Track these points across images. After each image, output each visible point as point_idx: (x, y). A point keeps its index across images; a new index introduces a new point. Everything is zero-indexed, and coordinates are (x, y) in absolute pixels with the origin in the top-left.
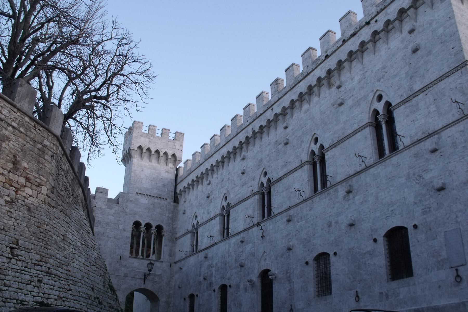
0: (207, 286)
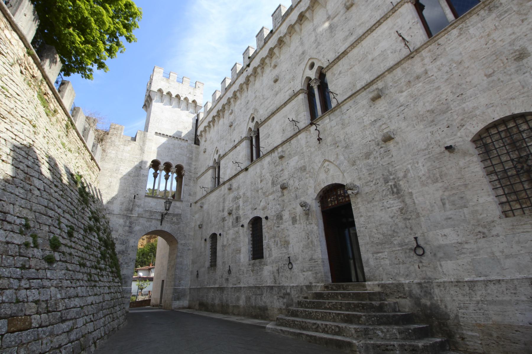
0: (233, 222)
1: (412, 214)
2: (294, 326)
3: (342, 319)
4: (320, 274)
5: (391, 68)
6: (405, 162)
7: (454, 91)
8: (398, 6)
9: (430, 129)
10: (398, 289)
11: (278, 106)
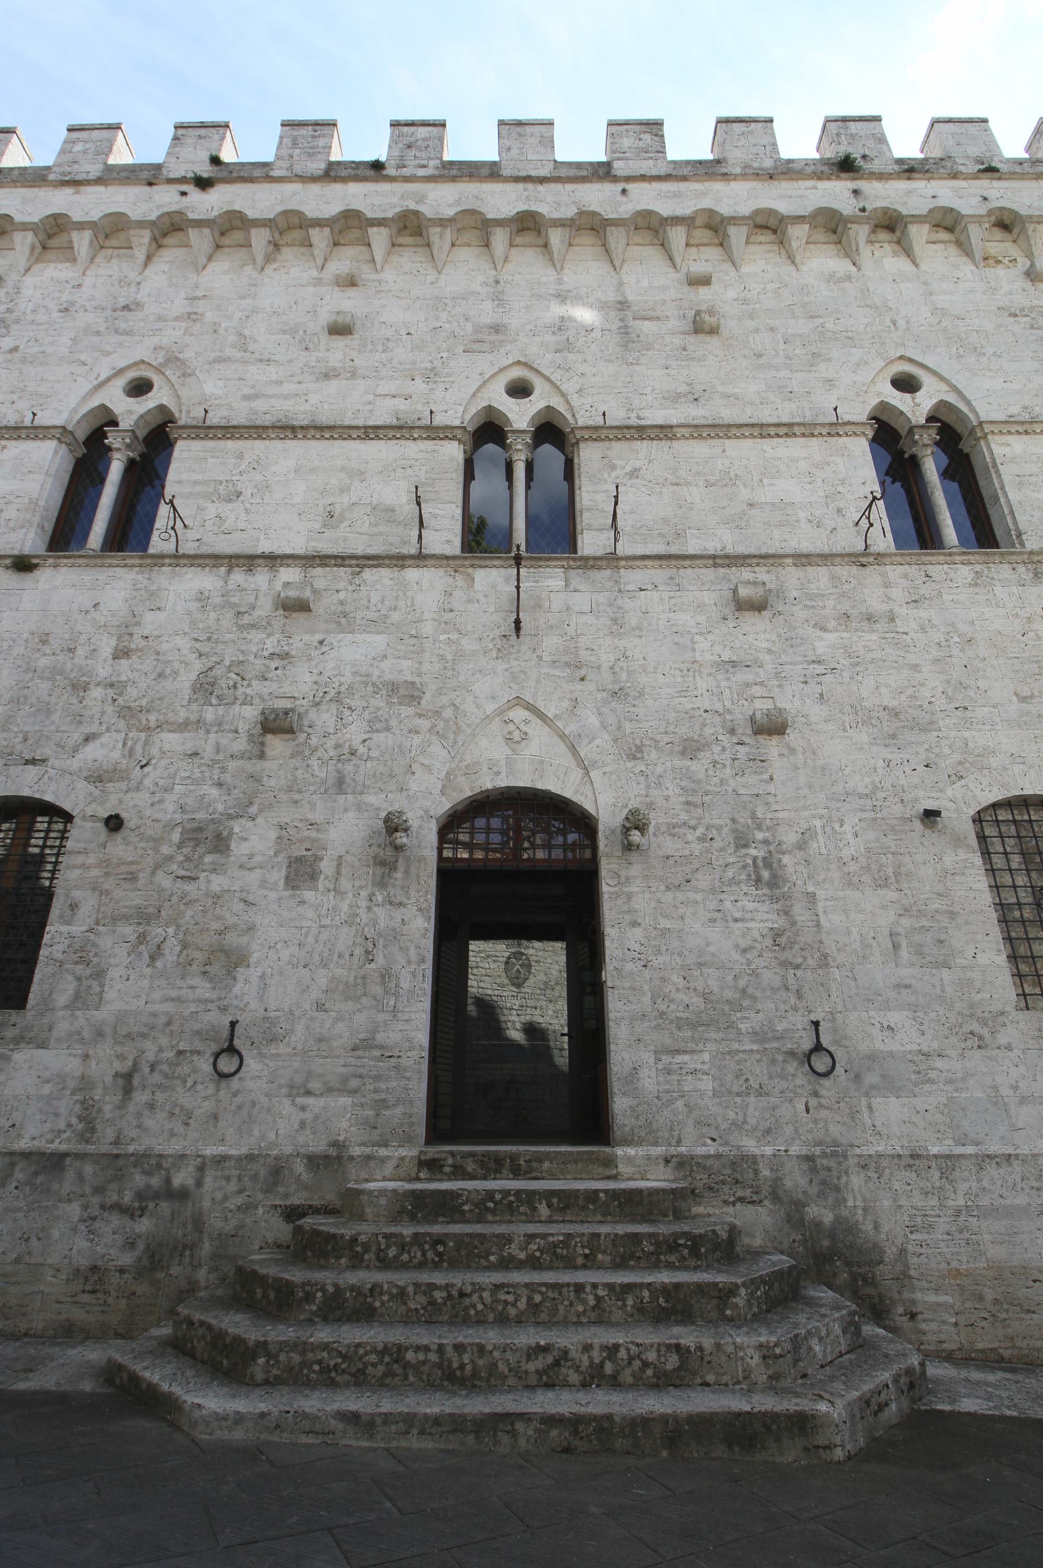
1: (806, 953)
2: (390, 1373)
3: (640, 1309)
4: (399, 1111)
5: (807, 556)
6: (805, 808)
7: (950, 691)
8: (847, 428)
9: (886, 753)
10: (737, 1175)
11: (325, 419)
